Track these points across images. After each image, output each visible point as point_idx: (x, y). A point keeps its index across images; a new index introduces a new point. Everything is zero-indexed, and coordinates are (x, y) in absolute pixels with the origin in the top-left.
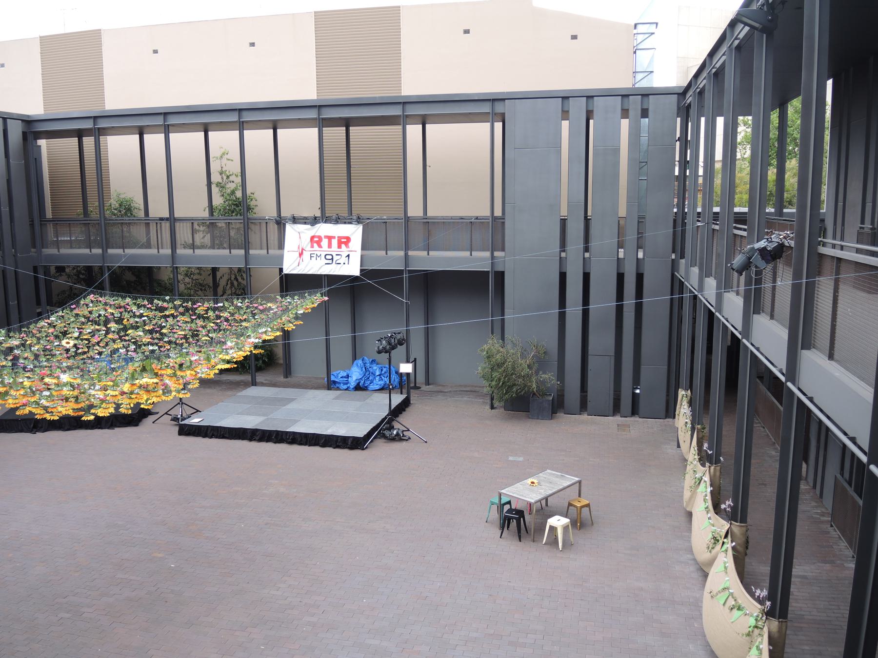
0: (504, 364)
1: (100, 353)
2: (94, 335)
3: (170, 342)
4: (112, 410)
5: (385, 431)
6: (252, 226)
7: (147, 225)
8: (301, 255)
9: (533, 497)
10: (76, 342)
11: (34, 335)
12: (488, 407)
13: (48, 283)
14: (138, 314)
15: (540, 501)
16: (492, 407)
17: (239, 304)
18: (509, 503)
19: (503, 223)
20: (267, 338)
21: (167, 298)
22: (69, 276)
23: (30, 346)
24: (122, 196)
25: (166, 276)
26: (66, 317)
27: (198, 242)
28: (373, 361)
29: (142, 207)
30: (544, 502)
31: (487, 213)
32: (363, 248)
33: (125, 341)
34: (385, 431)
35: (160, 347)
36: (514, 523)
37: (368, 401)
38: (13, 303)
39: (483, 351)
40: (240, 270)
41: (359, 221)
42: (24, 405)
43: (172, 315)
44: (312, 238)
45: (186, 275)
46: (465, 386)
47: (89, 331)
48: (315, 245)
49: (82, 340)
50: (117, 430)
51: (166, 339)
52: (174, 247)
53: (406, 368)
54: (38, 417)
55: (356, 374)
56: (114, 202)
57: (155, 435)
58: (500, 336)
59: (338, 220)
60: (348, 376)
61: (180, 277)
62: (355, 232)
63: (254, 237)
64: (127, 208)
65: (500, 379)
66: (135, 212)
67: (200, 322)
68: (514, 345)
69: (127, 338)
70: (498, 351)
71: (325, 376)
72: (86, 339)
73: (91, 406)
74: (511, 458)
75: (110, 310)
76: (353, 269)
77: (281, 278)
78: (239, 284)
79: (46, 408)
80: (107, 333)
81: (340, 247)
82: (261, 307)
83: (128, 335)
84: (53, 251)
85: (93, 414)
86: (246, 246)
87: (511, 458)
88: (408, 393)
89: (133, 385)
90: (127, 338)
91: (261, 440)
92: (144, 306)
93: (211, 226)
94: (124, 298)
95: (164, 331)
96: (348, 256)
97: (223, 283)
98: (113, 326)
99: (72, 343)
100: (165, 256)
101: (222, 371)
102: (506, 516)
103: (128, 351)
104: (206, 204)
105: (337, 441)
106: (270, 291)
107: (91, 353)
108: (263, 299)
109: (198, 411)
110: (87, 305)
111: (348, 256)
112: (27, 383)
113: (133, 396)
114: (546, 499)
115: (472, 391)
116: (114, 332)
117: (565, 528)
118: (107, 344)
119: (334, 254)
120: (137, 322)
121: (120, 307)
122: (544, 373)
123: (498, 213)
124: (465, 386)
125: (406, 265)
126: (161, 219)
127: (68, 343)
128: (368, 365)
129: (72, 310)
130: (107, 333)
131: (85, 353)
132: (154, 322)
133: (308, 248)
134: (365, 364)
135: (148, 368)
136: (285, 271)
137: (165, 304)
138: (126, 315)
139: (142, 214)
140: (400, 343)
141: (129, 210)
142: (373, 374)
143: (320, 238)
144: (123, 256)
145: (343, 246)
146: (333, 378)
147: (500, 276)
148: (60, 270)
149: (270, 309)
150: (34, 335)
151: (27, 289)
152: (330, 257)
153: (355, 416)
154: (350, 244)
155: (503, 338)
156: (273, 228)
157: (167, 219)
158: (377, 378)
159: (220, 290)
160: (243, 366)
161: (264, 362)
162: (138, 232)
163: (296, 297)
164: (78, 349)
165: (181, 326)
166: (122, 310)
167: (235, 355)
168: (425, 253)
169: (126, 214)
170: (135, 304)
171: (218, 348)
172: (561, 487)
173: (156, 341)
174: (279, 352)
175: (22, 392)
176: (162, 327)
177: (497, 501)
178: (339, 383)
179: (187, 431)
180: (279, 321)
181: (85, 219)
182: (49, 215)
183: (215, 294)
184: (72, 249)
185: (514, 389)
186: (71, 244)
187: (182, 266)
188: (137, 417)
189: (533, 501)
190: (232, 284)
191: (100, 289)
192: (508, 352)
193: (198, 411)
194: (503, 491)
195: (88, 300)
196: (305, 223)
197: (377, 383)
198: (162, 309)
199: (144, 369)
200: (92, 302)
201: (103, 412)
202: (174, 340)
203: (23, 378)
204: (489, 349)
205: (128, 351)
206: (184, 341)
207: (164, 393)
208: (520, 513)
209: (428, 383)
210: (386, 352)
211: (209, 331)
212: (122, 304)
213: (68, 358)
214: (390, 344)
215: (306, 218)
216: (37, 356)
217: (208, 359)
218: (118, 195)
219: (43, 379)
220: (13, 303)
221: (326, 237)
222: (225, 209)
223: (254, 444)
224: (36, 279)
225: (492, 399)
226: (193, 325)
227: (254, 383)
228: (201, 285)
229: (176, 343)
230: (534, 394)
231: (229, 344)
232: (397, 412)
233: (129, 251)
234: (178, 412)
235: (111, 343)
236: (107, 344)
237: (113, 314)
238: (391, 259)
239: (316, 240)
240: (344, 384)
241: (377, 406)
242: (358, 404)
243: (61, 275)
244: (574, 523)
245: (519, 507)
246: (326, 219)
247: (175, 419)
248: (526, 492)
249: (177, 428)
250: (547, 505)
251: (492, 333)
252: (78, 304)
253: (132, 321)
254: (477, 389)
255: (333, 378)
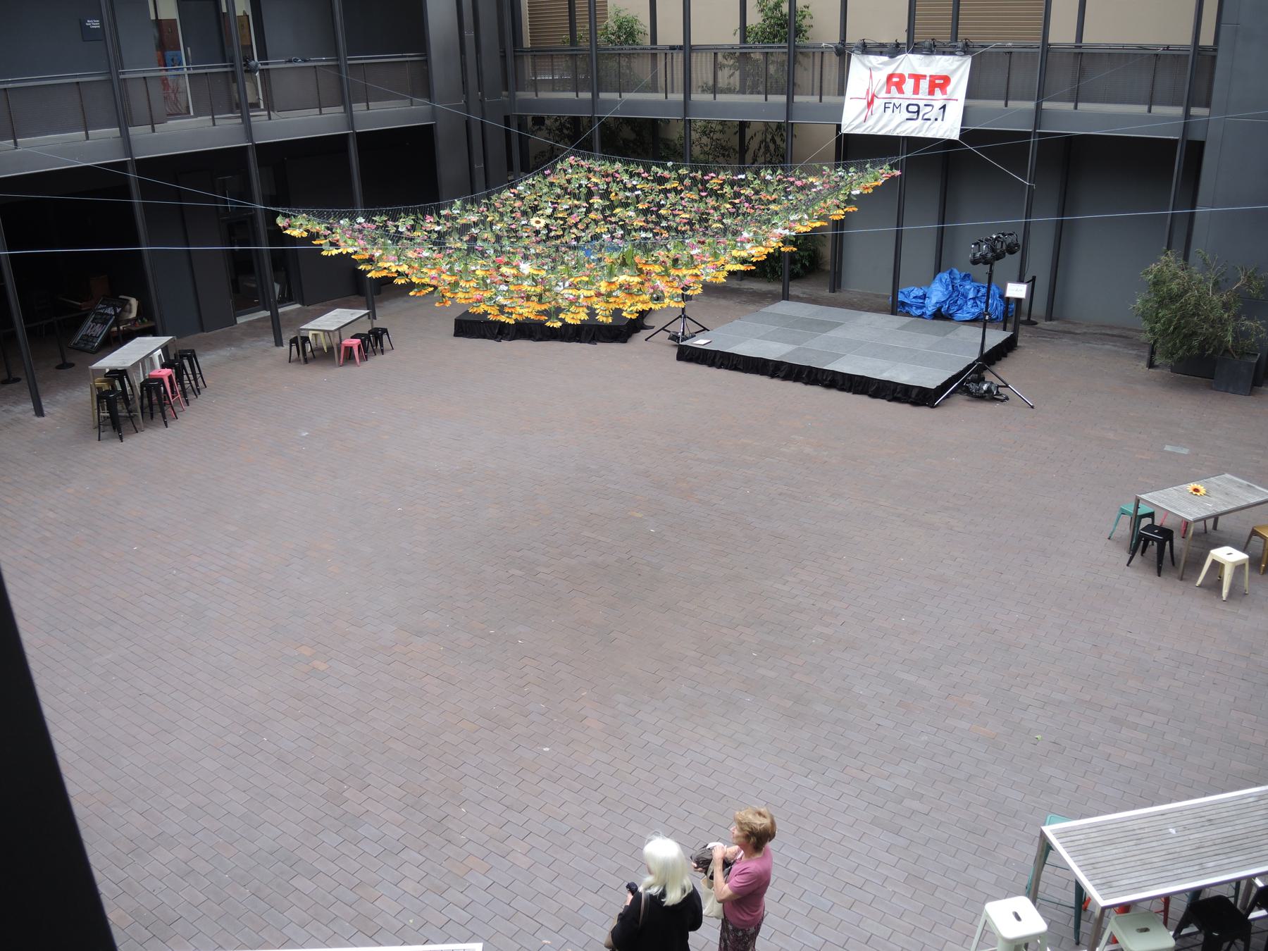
0: (1181, 296)
1: (578, 239)
2: (572, 213)
3: (668, 229)
4: (583, 316)
5: (970, 383)
6: (800, 58)
7: (654, 56)
8: (870, 104)
9: (1192, 512)
10: (548, 221)
11: (496, 210)
12: (1144, 364)
13: (523, 141)
14: (629, 186)
15: (1204, 519)
16: (1151, 365)
17: (768, 177)
18: (1151, 515)
19: (1214, 58)
20: (803, 229)
21: (670, 164)
22: (550, 131)
23: (491, 224)
24: (622, 14)
25: (675, 134)
26: (538, 186)
27: (722, 82)
28: (966, 277)
29: (648, 31)
30: (1210, 523)
31: (1186, 39)
32: (970, 94)
33: (611, 223)
34: (970, 383)
35: (655, 235)
36: (1153, 548)
37: (950, 336)
38: (479, 166)
39: (1147, 273)
40: (779, 125)
41: (966, 50)
42: (479, 301)
43: (675, 189)
44: (890, 77)
45: (704, 133)
46: (1111, 327)
47: (566, 207)
48: (893, 89)
49: (556, 219)
50: (599, 345)
51: (664, 224)
52: (687, 91)
53: (1017, 290)
54: (491, 318)
55: (937, 294)
56: (612, 25)
57: (647, 357)
58: (1181, 252)
59: (932, 49)
60: (924, 297)
61: (695, 136)
62: (958, 69)
63: (804, 76)
64: (627, 31)
65: (1170, 321)
66: (639, 38)
67: (712, 202)
68: (1206, 266)
69: (613, 219)
70: (1175, 276)
71: (890, 293)
72: (561, 219)
73: (559, 310)
74: (1168, 448)
75: (594, 180)
76: (948, 127)
77: (838, 140)
78: (777, 148)
79: (502, 308)
80: (588, 211)
81: (931, 92)
82: (798, 183)
83: (615, 215)
84: (528, 95)
85: (562, 320)
86: (790, 89)
87: (1168, 448)
88: (1016, 330)
89: (611, 283)
90: (613, 219)
91: (785, 378)
92: (639, 175)
93: (742, 57)
94: (613, 162)
95: (663, 212)
96: (944, 107)
97: (754, 145)
98: (597, 201)
99: (543, 222)
100: (676, 103)
101: (732, 274)
102: (1141, 536)
103: (613, 238)
104: (737, 24)
105: (894, 391)
106: (821, 159)
107: (567, 238)
108: (803, 170)
109: (705, 329)
110: (565, 171)
111: (944, 107)
112: (480, 273)
113: (611, 300)
114: (1216, 518)
115: (1118, 336)
116: (597, 210)
117: (1239, 568)
118: (587, 227)
119: (921, 104)
120: (627, 198)
121: (607, 176)
122: (1250, 318)
123: (1207, 39)
124: (1111, 327)
125: (1037, 124)
126: (673, 48)
127: (538, 222)
128: (958, 282)
129: (545, 177)
130: (588, 211)
131: (558, 237)
132: (650, 198)
133: (883, 94)
134: (953, 279)
135: (628, 262)
136: (844, 130)
137: (666, 174)
138: (614, 187)
139: (647, 41)
140: (1011, 250)
141: (631, 34)
142: (965, 296)
143: (902, 77)
144: (620, 102)
145: (937, 91)
146: (901, 298)
147: (1195, 150)
148: (539, 121)
149: (812, 185)
150: (496, 210)
151: (497, 147)
152: (915, 109)
153: (926, 356)
154: (949, 89)
155: (1186, 258)
156: (832, 61)
157: (680, 48)
158: (970, 303)
159: (749, 156)
160: (768, 268)
161: (803, 266)
162: (642, 68)
163: (852, 169)
164: (550, 231)
165: (686, 206)
166: (610, 179)
167: (753, 252)
168: (1069, 106)
169: (626, 41)
170: (626, 171)
171: (728, 240)
172: (1244, 504)
173: (651, 226)
174: (827, 251)
175: (473, 284)
176: (660, 206)
177: (1131, 509)
178: (911, 306)
179: (689, 355)
180: (822, 204)
181: (572, 52)
182: (527, 43)
183: (742, 161)
184: (554, 93)
185: (1195, 343)
186: (553, 86)
187: (698, 119)
188: (620, 331)
189: (1191, 518)
190: (767, 147)
191: (585, 148)
192: (1191, 277)
193: (705, 329)
194: (1143, 496)
195: (566, 165)
196: (881, 54)
197: (970, 311)
198: (661, 180)
199: (624, 264)
200: (572, 166)
201: (576, 317)
202: (674, 225)
203: (476, 264)
204: (1159, 271)
205: (613, 238)
206: (688, 227)
207: (652, 299)
208: (1167, 534)
209: (1049, 316)
210: (986, 263)
211: (723, 215)
212: (610, 171)
213: (538, 242)
214: (993, 250)
215: (882, 45)
216: (498, 238)
217: (715, 255)
218: (617, 13)
219: (499, 267)
220: (479, 166)
221: (911, 76)
222: (763, 32)
223: (776, 383)
224: (508, 133)
225: (1153, 352)
226: (702, 206)
227: (786, 296)
228: (723, 148)
229: (676, 230)
230: (1227, 350)
231: (745, 234)
232: (991, 358)
233: (627, 96)
234: (678, 328)
235: (592, 226)
236: (587, 227)
237: (596, 185)
238: (1013, 114)
239: (896, 82)
240: (918, 308)
241: (963, 346)
242: (935, 339)
243: (540, 129)
244: (1255, 562)
245: (1168, 523)
246: (913, 46)
247: (674, 338)
248: (1183, 503)
249: (676, 350)
250: (1215, 527)
251: (1169, 248)
252: (553, 169)
253: (621, 195)
254: (1131, 333)
255: (901, 298)
